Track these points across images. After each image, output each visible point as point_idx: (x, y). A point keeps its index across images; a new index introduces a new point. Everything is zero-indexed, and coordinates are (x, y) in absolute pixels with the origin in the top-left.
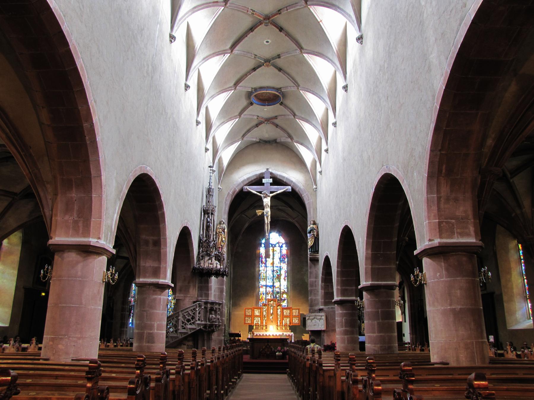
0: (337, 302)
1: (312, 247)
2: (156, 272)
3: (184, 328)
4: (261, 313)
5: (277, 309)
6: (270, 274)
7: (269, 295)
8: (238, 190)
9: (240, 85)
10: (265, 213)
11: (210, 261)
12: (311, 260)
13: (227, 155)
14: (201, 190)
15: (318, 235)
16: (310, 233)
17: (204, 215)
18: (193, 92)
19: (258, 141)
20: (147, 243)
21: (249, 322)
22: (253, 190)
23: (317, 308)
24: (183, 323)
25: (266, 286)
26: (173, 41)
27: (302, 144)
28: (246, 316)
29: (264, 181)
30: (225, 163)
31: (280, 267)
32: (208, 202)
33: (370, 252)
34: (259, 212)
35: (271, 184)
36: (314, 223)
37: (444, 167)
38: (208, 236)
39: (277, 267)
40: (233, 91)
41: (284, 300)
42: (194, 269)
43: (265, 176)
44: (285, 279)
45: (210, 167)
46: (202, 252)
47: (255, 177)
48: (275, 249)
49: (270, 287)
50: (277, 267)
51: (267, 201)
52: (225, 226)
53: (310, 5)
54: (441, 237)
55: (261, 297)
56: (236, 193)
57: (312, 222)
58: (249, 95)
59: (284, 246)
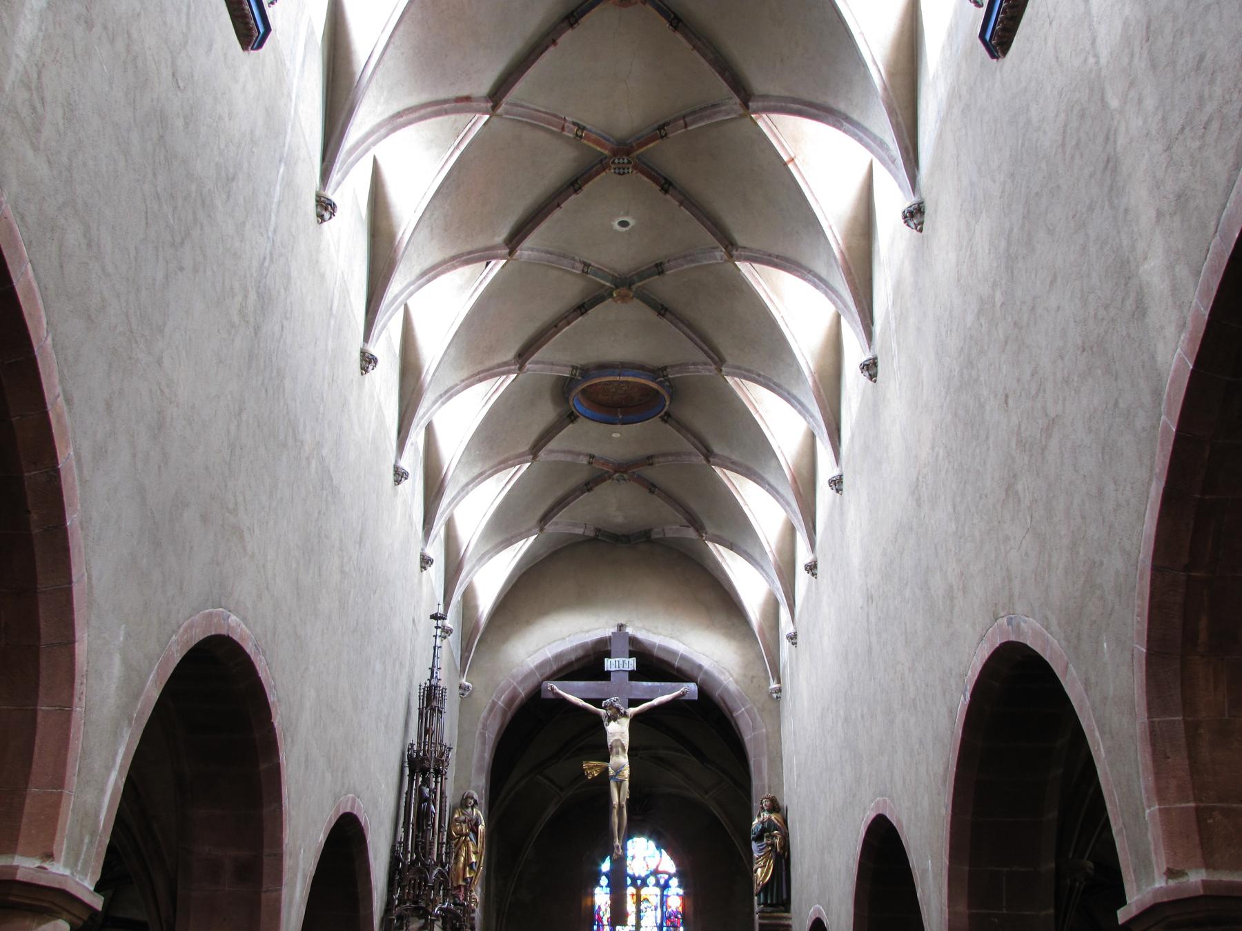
1: (766, 888)
8: (523, 692)
9: (536, 356)
10: (611, 772)
13: (490, 579)
15: (786, 845)
16: (759, 838)
18: (386, 376)
19: (591, 533)
22: (574, 694)
26: (327, 215)
27: (731, 546)
29: (610, 664)
30: (485, 603)
32: (427, 731)
33: (962, 908)
35: (633, 676)
36: (775, 807)
37: (1203, 623)
38: (422, 847)
40: (513, 376)
43: (614, 648)
45: (435, 617)
46: (401, 901)
47: (580, 653)
48: (645, 892)
51: (618, 731)
52: (479, 813)
53: (755, 112)
54: (1208, 865)
56: (517, 702)
57: (766, 803)
58: (563, 389)
59: (674, 882)
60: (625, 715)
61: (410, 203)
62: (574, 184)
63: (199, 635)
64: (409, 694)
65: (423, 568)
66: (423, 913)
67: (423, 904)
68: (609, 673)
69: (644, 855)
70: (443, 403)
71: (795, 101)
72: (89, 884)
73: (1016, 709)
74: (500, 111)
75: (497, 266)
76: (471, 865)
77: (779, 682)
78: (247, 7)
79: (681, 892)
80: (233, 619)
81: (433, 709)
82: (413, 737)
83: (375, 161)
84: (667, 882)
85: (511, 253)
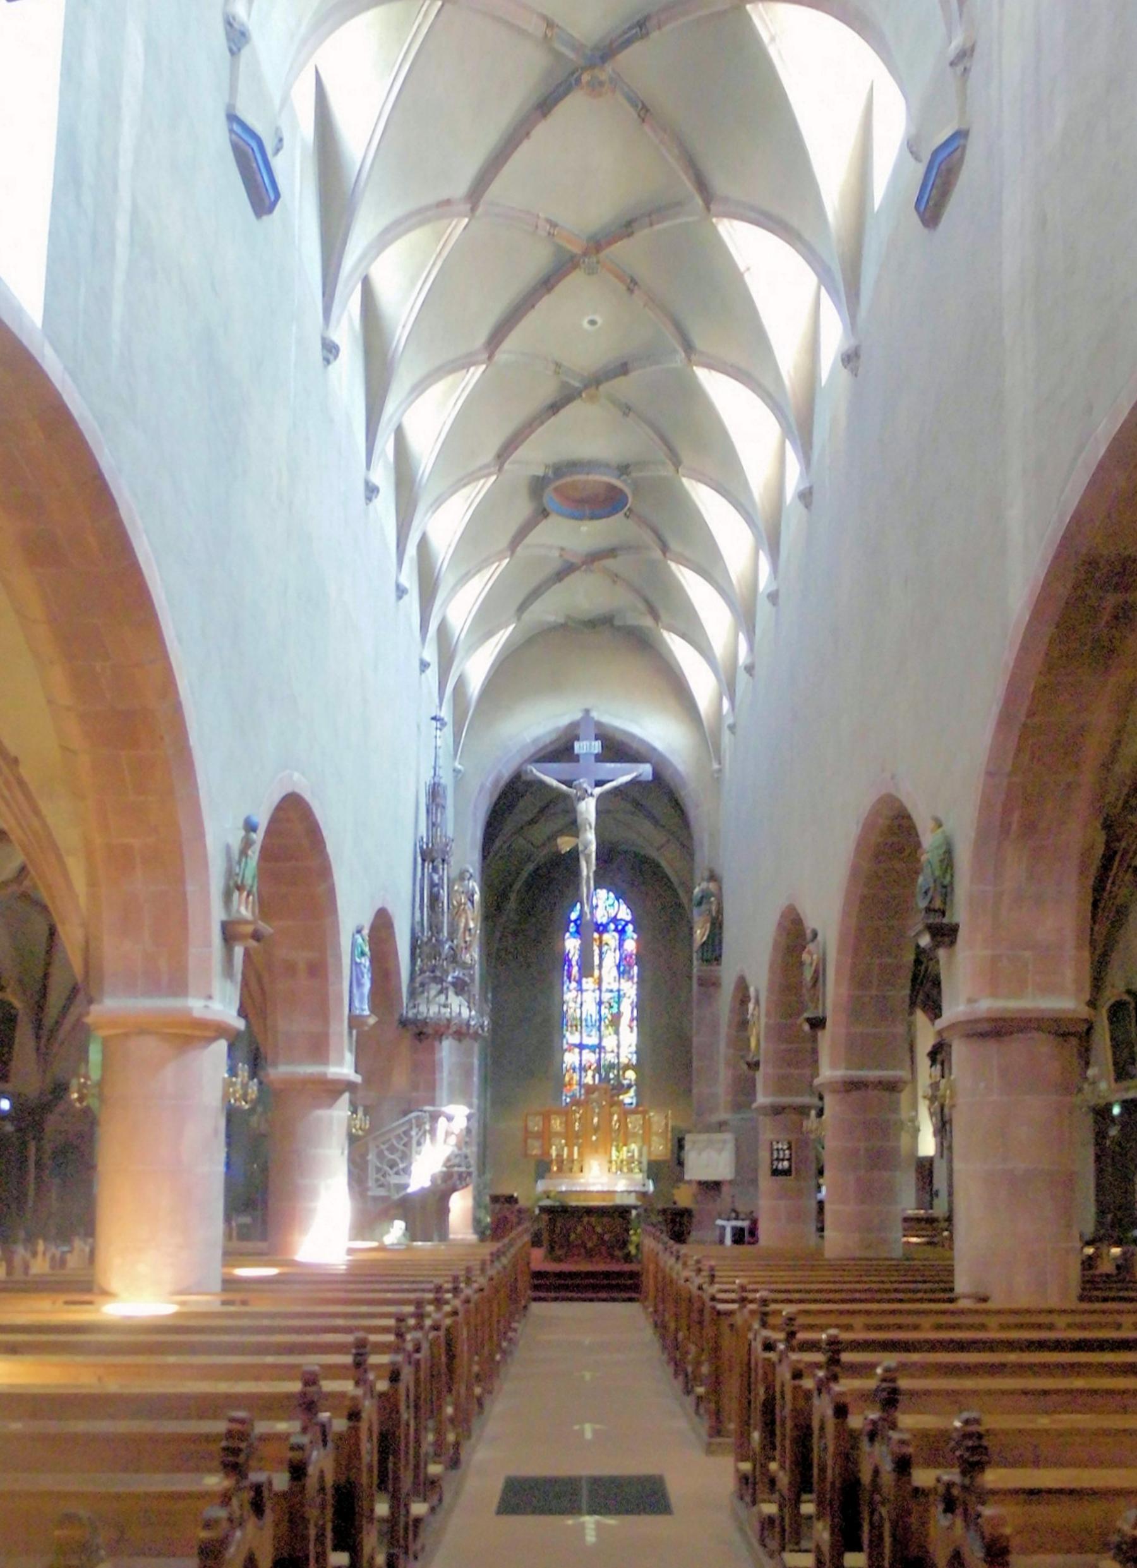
0: (763, 1110)
2: (319, 1048)
3: (382, 1186)
4: (568, 1124)
5: (611, 1115)
6: (590, 1008)
7: (590, 1073)
8: (507, 774)
9: (511, 458)
10: (581, 848)
11: (442, 997)
12: (702, 983)
13: (477, 667)
14: (413, 790)
15: (720, 911)
17: (423, 865)
18: (348, 372)
19: (561, 620)
20: (290, 969)
21: (536, 1152)
22: (549, 776)
23: (715, 1118)
24: (378, 1170)
25: (581, 1047)
26: (331, 357)
27: (683, 636)
28: (527, 1133)
29: (580, 747)
31: (619, 991)
32: (434, 824)
34: (565, 844)
35: (599, 758)
36: (713, 877)
37: (1016, 816)
38: (435, 928)
39: (611, 991)
40: (493, 478)
41: (630, 1086)
42: (404, 1023)
43: (581, 732)
44: (631, 1028)
45: (434, 718)
46: (422, 971)
47: (554, 736)
48: (606, 937)
49: (593, 1048)
50: (611, 991)
51: (588, 809)
52: (474, 885)
53: (717, 216)
54: (994, 995)
55: (567, 1079)
57: (706, 874)
58: (538, 486)
59: (630, 928)
60: (592, 795)
61: (401, 303)
62: (547, 283)
63: (276, 798)
64: (417, 792)
65: (422, 671)
66: (441, 980)
67: (438, 974)
68: (578, 756)
69: (605, 905)
70: (434, 512)
71: (752, 208)
72: (234, 1012)
73: (892, 844)
74: (480, 211)
75: (476, 373)
76: (470, 930)
77: (720, 763)
78: (254, 165)
79: (635, 936)
80: (296, 776)
81: (437, 806)
82: (423, 830)
83: (317, 72)
84: (624, 927)
85: (490, 357)
